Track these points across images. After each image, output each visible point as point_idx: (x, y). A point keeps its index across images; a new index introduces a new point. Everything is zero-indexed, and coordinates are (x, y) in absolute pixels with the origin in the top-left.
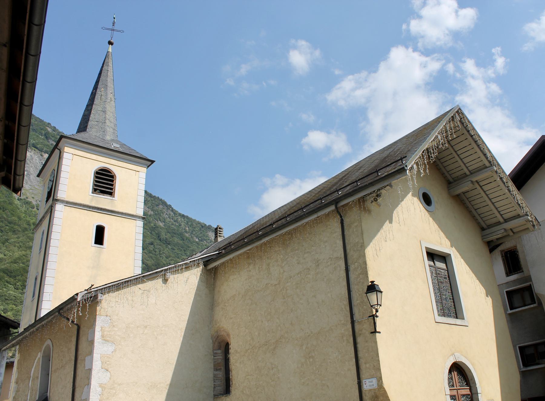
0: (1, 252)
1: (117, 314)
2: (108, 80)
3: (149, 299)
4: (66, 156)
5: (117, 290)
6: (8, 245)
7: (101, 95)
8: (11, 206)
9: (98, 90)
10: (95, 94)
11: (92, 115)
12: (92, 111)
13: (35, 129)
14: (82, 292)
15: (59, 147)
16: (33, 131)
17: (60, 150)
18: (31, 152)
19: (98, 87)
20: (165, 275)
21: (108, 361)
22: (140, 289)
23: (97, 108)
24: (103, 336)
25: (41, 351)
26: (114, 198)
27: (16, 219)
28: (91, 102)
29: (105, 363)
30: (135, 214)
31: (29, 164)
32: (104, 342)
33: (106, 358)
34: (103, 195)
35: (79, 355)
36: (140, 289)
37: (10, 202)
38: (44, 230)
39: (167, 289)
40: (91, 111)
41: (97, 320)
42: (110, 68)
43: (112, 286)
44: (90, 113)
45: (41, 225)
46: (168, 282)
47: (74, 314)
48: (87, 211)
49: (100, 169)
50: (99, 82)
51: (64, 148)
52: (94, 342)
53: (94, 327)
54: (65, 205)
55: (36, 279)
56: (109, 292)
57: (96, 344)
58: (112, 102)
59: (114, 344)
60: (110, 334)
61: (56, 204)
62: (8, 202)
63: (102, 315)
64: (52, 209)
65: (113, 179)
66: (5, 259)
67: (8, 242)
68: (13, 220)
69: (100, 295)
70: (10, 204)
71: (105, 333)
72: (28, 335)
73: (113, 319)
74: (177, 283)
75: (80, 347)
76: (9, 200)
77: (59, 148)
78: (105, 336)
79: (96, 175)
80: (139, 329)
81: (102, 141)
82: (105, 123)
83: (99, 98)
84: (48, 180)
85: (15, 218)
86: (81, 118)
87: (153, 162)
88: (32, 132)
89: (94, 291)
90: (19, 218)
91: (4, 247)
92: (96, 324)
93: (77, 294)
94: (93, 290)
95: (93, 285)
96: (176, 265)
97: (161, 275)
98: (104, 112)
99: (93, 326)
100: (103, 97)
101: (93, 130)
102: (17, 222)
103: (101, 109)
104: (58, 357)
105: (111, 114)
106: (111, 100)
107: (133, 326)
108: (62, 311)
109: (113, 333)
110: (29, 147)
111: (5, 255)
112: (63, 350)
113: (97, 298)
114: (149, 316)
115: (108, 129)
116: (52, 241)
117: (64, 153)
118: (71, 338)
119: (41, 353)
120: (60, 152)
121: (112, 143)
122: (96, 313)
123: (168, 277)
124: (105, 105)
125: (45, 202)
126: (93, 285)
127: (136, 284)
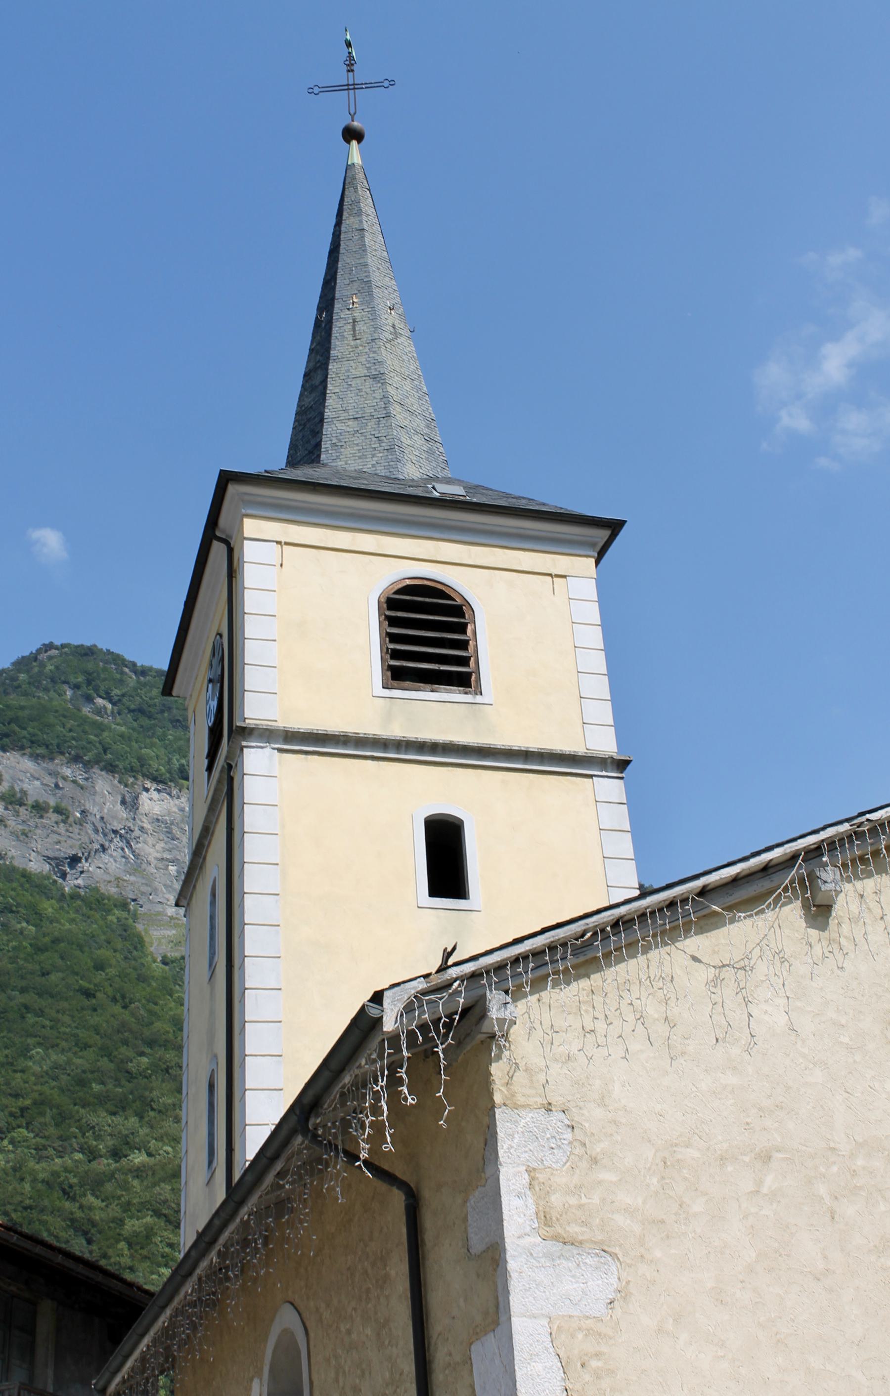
0: (138, 1146)
1: (603, 1098)
2: (369, 261)
3: (752, 1009)
4: (250, 552)
5: (582, 971)
6: (155, 1118)
7: (354, 321)
8: (144, 989)
9: (337, 306)
10: (330, 322)
11: (331, 401)
12: (330, 387)
13: (181, 719)
14: (397, 985)
15: (223, 532)
16: (174, 727)
17: (226, 542)
18: (178, 798)
19: (337, 295)
20: (813, 878)
21: (598, 1355)
22: (695, 959)
23: (348, 371)
24: (545, 1218)
25: (259, 1373)
26: (478, 699)
27: (168, 1029)
28: (318, 357)
29: (583, 1365)
30: (579, 749)
31: (178, 839)
32: (556, 1247)
33: (580, 1336)
34: (432, 691)
35: (433, 1341)
36: (695, 959)
37: (139, 975)
38: (215, 878)
39: (836, 951)
40: (325, 388)
41: (501, 1135)
42: (369, 219)
43: (552, 948)
44: (324, 394)
45: (201, 868)
46: (832, 922)
47: (376, 1110)
48: (375, 763)
49: (400, 586)
50: (338, 252)
51: (242, 521)
52: (504, 1250)
53: (489, 1171)
54: (280, 750)
55: (211, 1087)
56: (538, 984)
57: (515, 1263)
58: (399, 341)
59: (614, 1256)
60: (580, 1206)
61: (245, 750)
62: (134, 975)
63: (523, 1106)
64: (231, 780)
65: (462, 620)
66: (151, 1168)
67: (153, 1109)
68: (158, 1031)
69: (495, 999)
70: (143, 982)
71: (553, 1198)
72: (191, 1294)
73: (587, 1125)
74: (882, 918)
75: (435, 1299)
76: (135, 969)
77: (224, 536)
78: (554, 1215)
79: (388, 613)
80: (730, 1169)
81: (390, 482)
82: (388, 416)
83: (348, 335)
84: (206, 681)
85: (165, 1026)
86: (292, 426)
87: (615, 527)
88: (170, 732)
89: (461, 978)
90: (175, 1025)
91: (144, 1128)
92: (501, 1153)
93: (377, 998)
94: (453, 972)
95: (454, 949)
96: (860, 825)
97: (792, 882)
98: (374, 377)
99: (483, 1171)
100: (360, 327)
101: (347, 451)
102: (171, 1036)
103: (363, 371)
104: (337, 1380)
105: (407, 386)
106: (396, 335)
107: (696, 1154)
108: (317, 1116)
109: (596, 1200)
110: (171, 781)
111: (150, 1155)
112: (354, 1336)
113: (483, 1015)
114: (770, 1096)
115: (403, 439)
116: (249, 901)
117: (245, 542)
118: (385, 1266)
119: (261, 1380)
120: (230, 551)
121: (430, 486)
122: (490, 1095)
123: (830, 886)
124: (374, 352)
125: (206, 774)
126: (454, 949)
127: (671, 935)
